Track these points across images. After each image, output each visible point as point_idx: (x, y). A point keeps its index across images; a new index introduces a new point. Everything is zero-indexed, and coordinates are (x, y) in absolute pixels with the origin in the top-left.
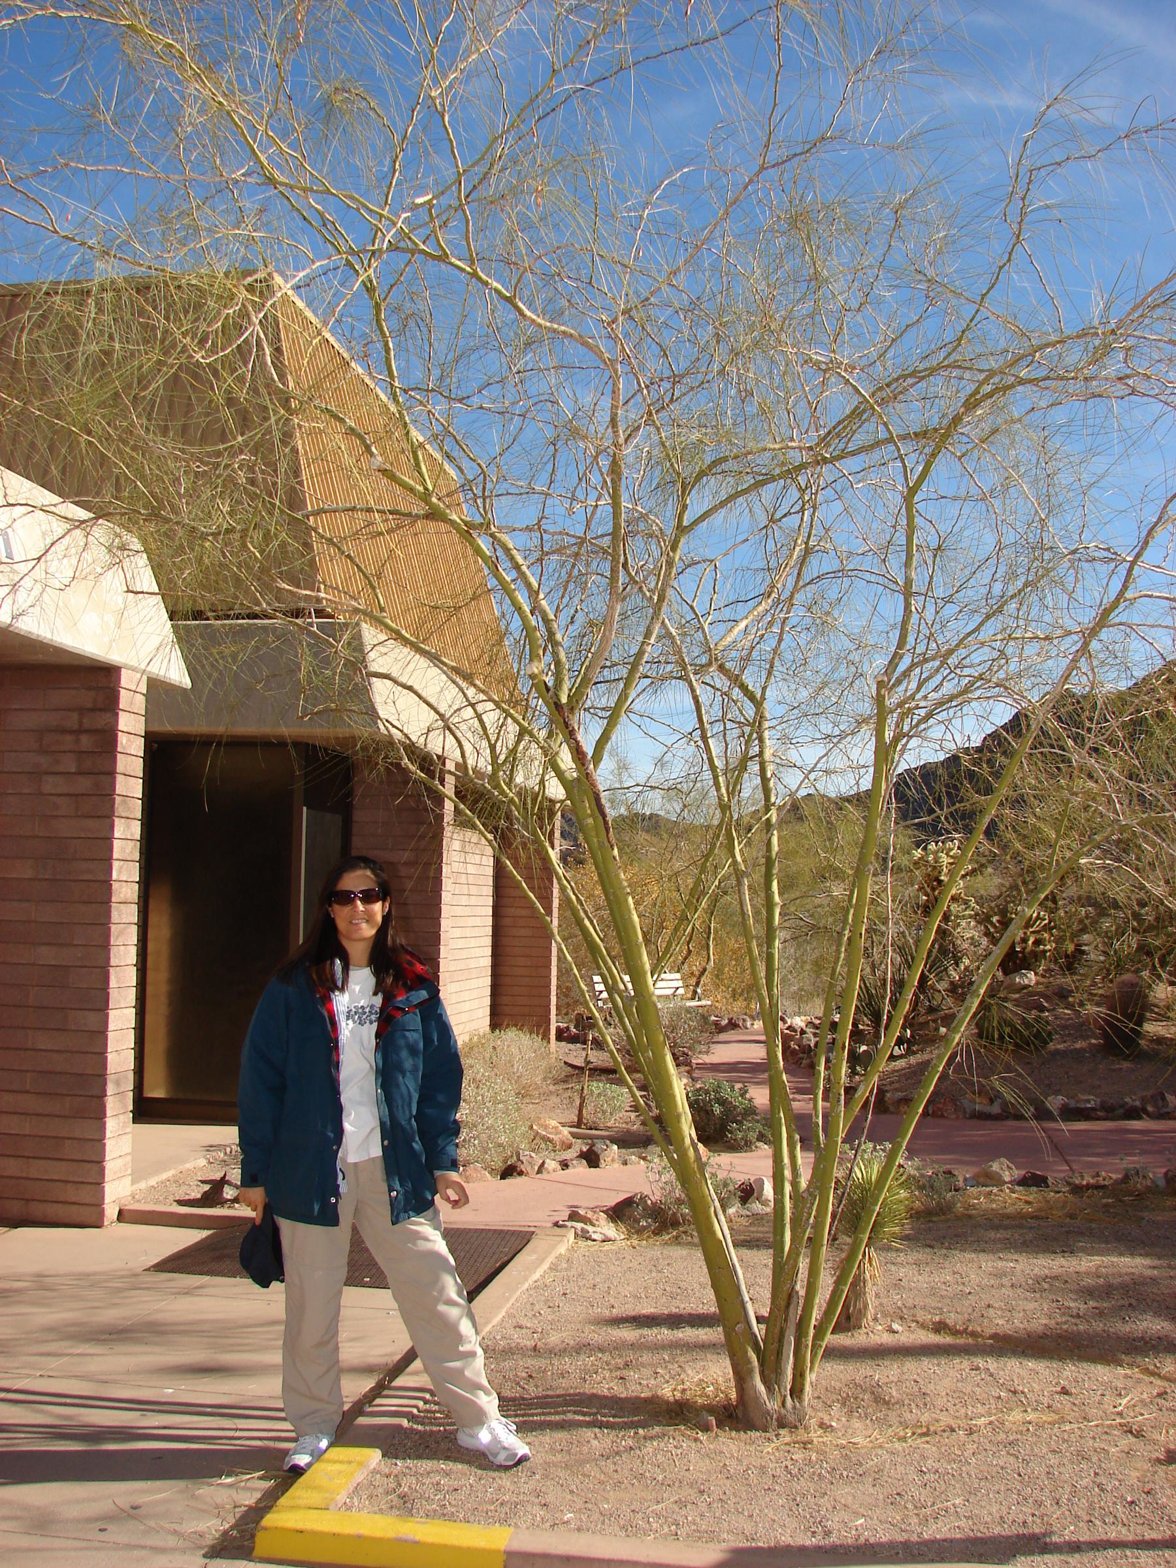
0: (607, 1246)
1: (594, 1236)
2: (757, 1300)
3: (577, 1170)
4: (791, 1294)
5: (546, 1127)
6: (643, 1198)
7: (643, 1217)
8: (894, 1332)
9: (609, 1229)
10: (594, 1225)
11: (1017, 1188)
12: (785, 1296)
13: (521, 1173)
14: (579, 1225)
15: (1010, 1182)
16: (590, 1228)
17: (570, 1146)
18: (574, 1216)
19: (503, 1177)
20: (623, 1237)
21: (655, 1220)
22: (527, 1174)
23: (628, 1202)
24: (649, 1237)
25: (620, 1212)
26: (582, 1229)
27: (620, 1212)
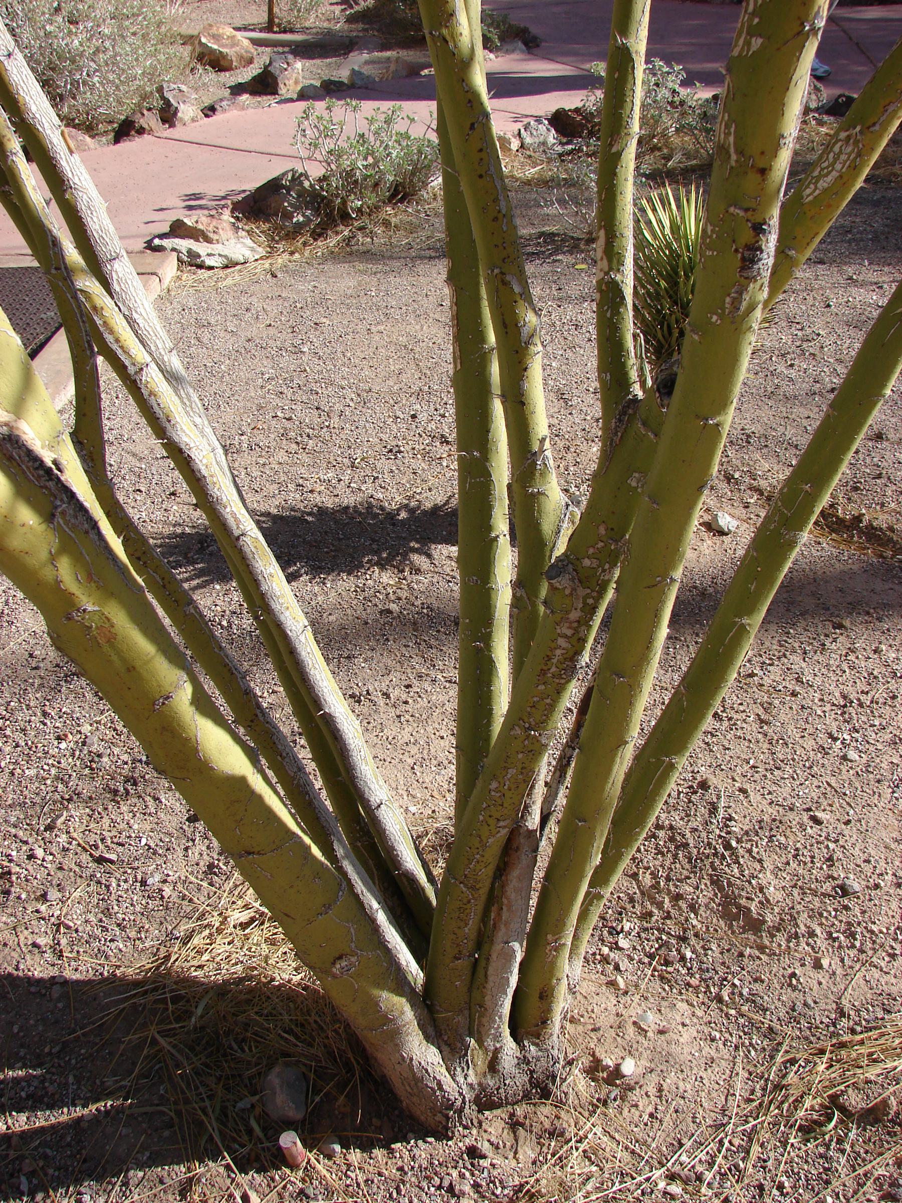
0: (233, 278)
1: (209, 262)
2: (409, 792)
3: (227, 115)
4: (517, 844)
5: (216, 38)
6: (297, 179)
7: (297, 208)
8: (722, 533)
9: (237, 244)
10: (208, 240)
11: (826, 118)
12: (496, 841)
13: (141, 131)
14: (184, 244)
15: (817, 110)
16: (201, 248)
17: (250, 61)
18: (178, 229)
19: (117, 141)
20: (261, 251)
21: (317, 211)
22: (151, 132)
23: (273, 187)
24: (305, 244)
25: (259, 207)
26: (190, 251)
27: (259, 207)
